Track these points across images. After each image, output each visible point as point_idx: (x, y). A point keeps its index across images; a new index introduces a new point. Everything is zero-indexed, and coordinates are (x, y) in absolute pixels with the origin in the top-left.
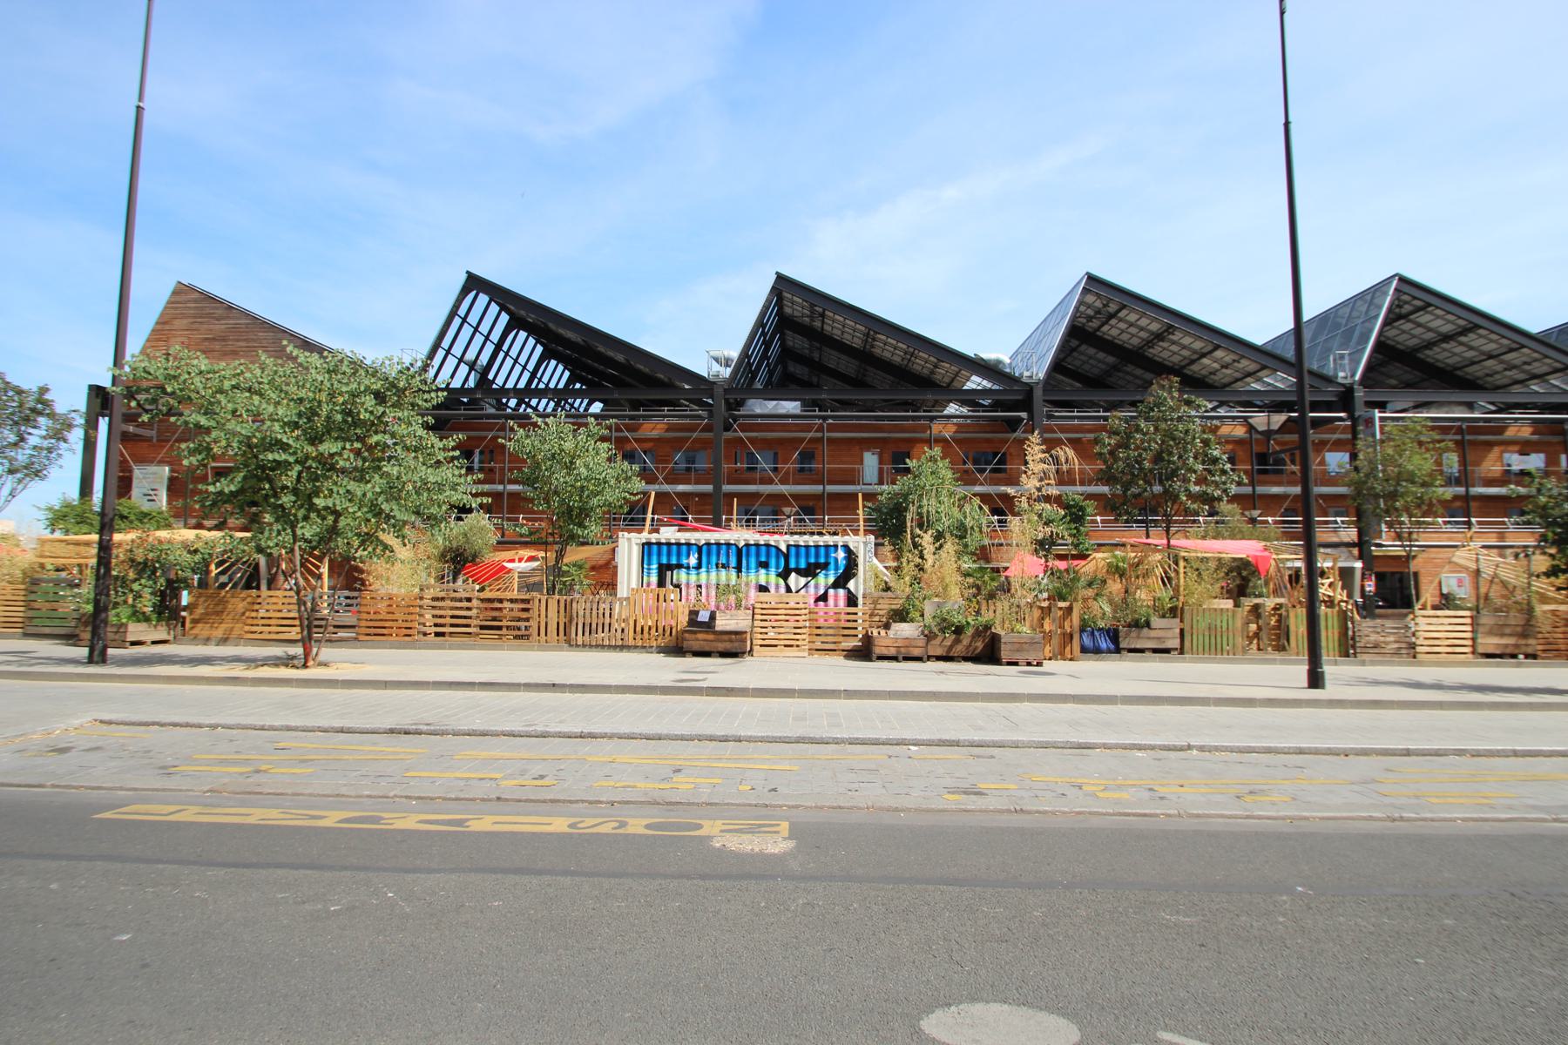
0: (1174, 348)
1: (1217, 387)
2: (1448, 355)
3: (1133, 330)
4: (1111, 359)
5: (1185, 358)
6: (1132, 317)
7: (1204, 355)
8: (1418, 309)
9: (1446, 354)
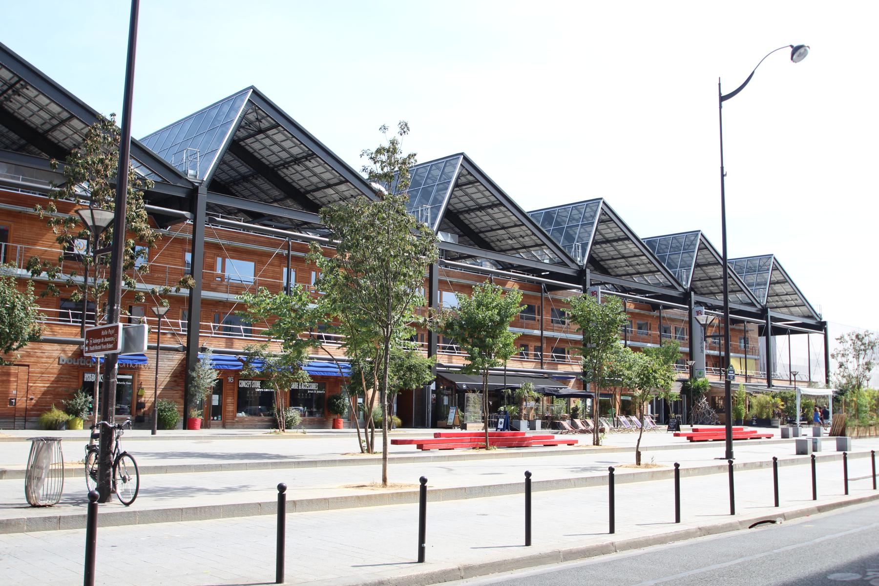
0: (307, 173)
2: (298, 175)
3: (276, 148)
4: (244, 169)
5: (312, 184)
6: (279, 137)
7: (329, 186)
8: (470, 183)
9: (478, 220)
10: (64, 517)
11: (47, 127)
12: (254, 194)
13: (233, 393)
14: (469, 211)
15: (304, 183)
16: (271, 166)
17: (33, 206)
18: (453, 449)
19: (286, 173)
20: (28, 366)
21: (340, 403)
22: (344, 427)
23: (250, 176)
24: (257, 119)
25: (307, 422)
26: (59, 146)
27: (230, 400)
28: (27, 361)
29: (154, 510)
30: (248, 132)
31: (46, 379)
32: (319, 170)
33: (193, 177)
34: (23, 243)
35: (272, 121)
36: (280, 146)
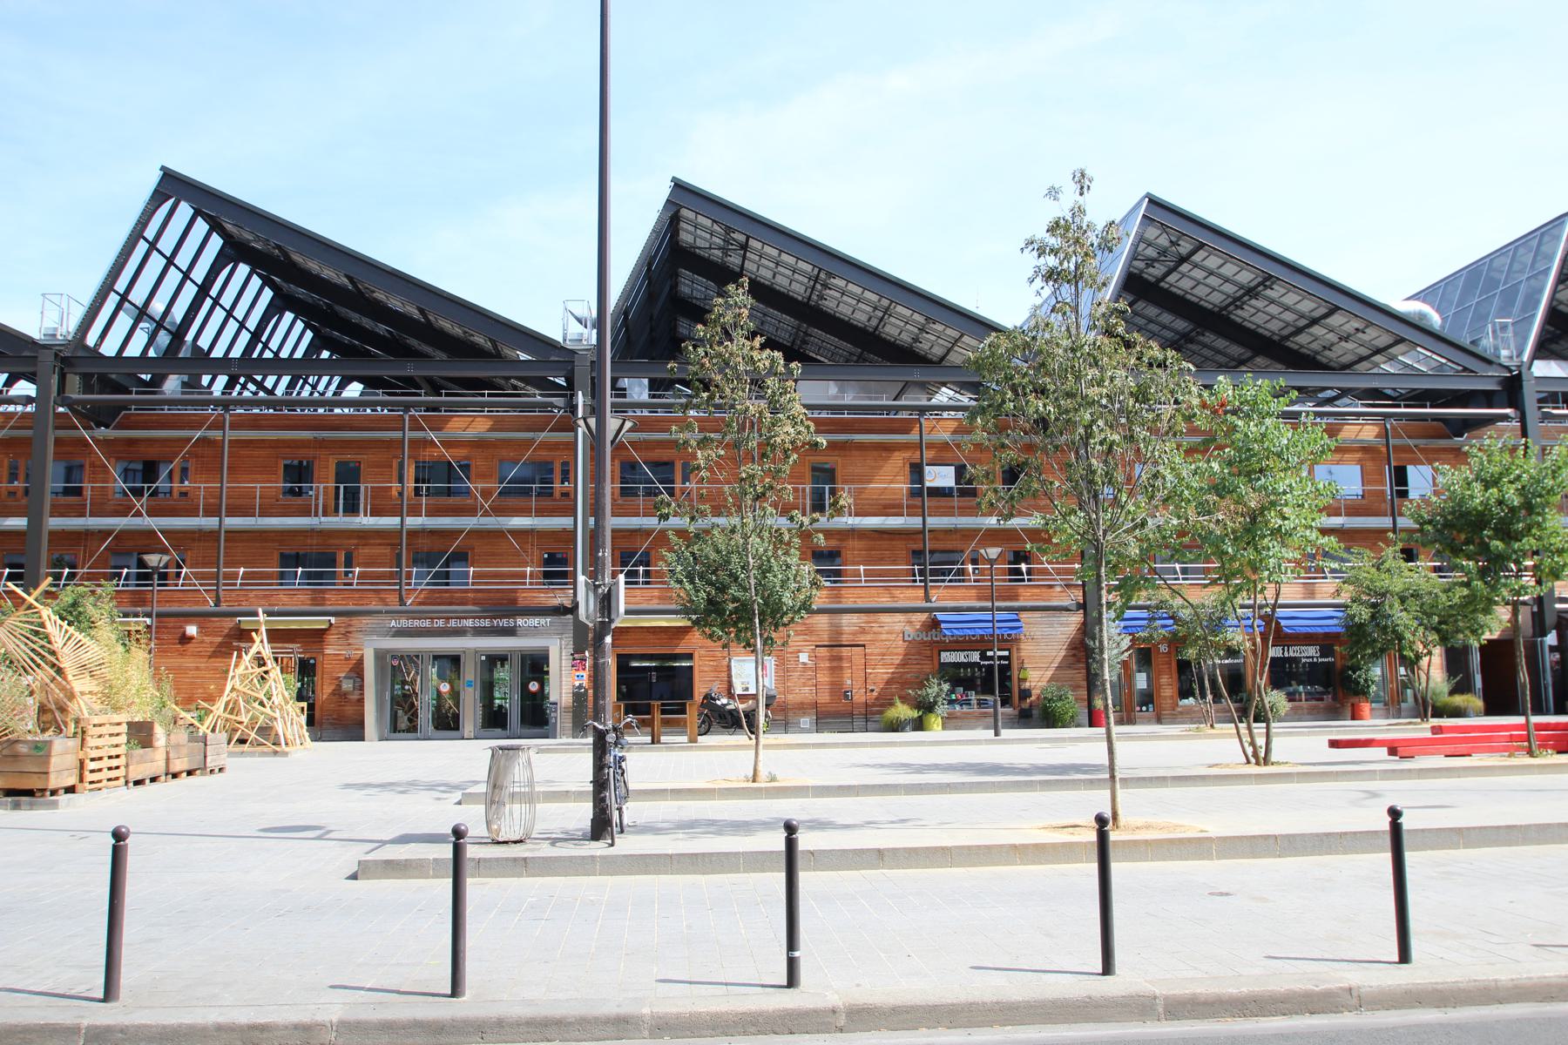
0: (1273, 309)
1: (931, 362)
3: (1213, 281)
6: (1213, 262)
7: (1315, 322)
10: (485, 860)
11: (874, 322)
12: (1207, 359)
13: (1170, 668)
15: (1275, 326)
17: (668, 430)
18: (1470, 755)
20: (864, 646)
21: (1360, 676)
22: (1373, 717)
24: (1171, 242)
25: (1306, 711)
27: (1164, 680)
28: (862, 639)
29: (624, 856)
31: (889, 662)
34: (852, 482)
36: (1219, 276)
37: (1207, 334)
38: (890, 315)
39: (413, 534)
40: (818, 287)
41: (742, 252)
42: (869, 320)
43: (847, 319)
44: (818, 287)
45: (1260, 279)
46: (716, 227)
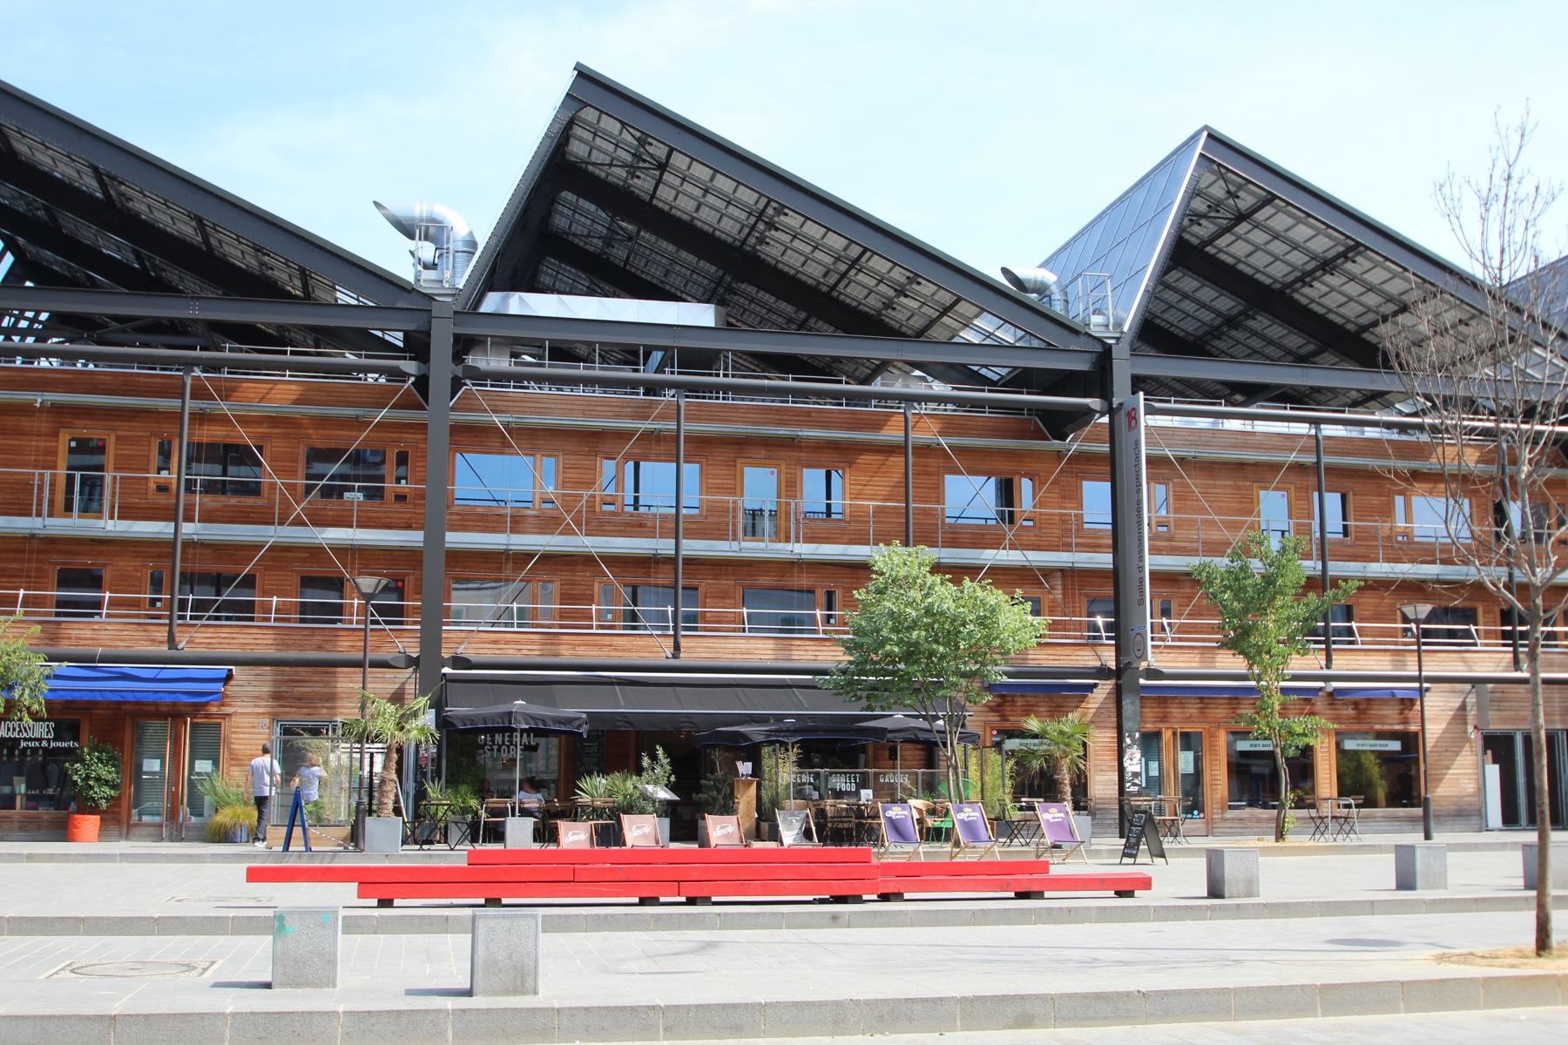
0: (1353, 289)
1: (904, 335)
3: (1278, 247)
4: (1226, 303)
6: (1280, 222)
11: (832, 280)
14: (1305, 278)
15: (1351, 311)
16: (1278, 286)
19: (1305, 295)
23: (1240, 313)
24: (1229, 192)
25: (16, 825)
26: (860, 311)
30: (1215, 224)
32: (1376, 277)
33: (1102, 329)
35: (1259, 191)
37: (1260, 318)
38: (860, 270)
39: (189, 544)
40: (761, 226)
41: (657, 173)
42: (825, 276)
43: (792, 272)
44: (761, 226)
45: (1341, 249)
46: (626, 136)
